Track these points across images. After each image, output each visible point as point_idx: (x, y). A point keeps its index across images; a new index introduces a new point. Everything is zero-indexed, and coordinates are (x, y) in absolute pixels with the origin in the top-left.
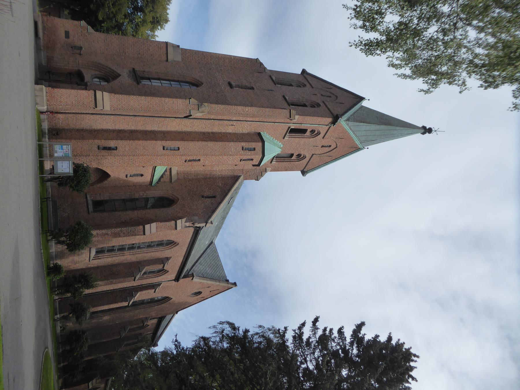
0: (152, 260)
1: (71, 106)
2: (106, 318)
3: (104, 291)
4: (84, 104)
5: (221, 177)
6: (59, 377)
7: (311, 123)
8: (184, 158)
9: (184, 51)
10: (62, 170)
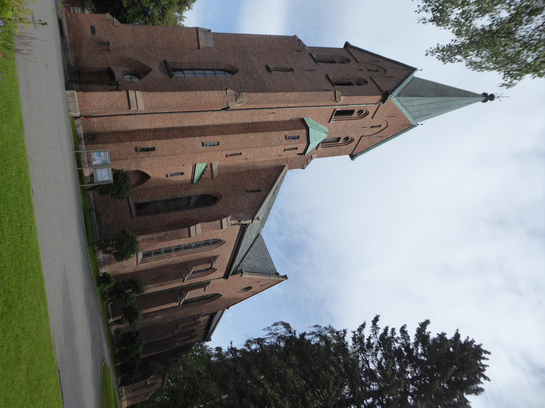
0: (199, 260)
1: (105, 109)
2: (158, 317)
3: (154, 293)
4: (118, 106)
5: (264, 168)
6: (117, 376)
7: (358, 104)
8: (225, 153)
9: (216, 35)
10: (102, 178)
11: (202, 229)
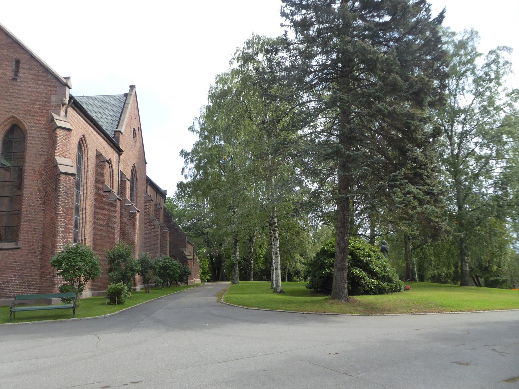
11: (64, 157)
